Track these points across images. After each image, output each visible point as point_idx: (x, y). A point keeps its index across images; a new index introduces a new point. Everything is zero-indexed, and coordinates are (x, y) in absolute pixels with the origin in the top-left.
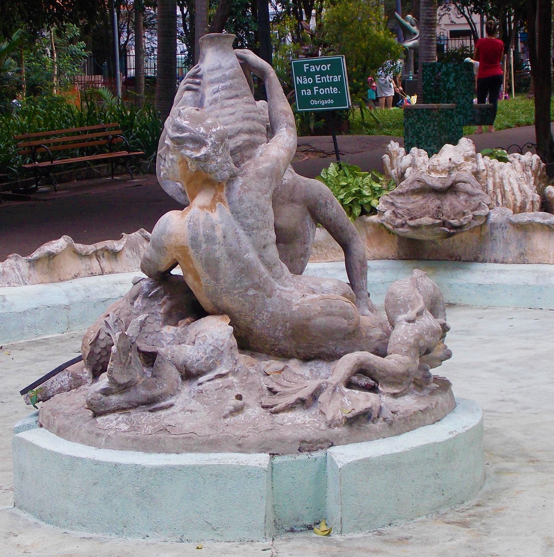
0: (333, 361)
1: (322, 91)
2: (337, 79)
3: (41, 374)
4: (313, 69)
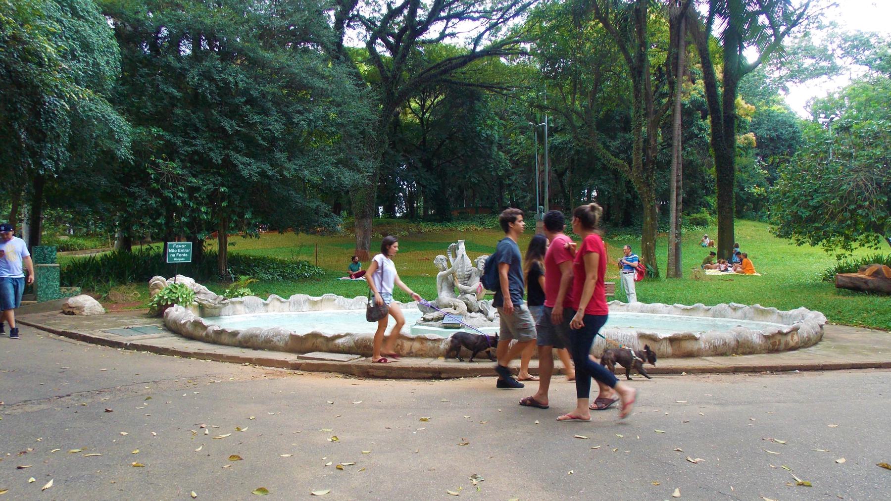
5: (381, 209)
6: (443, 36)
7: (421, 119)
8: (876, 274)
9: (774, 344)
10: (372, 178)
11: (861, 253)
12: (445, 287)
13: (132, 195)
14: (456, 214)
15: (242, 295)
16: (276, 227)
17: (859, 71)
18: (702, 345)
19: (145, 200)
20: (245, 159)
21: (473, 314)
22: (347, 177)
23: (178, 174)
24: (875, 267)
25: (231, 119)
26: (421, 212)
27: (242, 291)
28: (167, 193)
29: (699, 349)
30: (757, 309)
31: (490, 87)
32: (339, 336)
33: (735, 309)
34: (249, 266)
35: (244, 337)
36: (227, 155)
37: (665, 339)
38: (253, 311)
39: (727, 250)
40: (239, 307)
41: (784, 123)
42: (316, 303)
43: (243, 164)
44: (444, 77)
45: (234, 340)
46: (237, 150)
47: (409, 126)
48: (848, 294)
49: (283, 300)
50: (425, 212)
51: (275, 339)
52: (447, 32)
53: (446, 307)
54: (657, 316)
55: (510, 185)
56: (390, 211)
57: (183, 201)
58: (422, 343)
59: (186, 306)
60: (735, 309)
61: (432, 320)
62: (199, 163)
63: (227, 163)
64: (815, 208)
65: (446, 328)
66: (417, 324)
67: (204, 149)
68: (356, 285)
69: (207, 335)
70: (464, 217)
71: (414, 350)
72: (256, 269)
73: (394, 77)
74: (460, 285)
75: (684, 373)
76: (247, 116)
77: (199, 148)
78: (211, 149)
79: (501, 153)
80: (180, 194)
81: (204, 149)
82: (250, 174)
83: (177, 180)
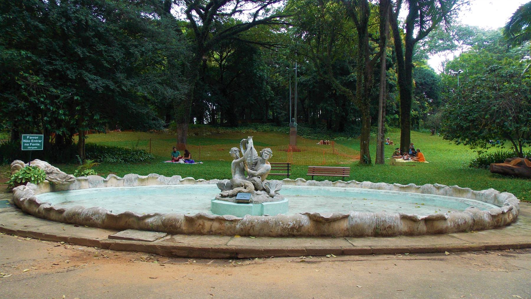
0: (413, 217)
1: (33, 145)
2: (40, 141)
3: (388, 240)
4: (31, 138)
5: (195, 119)
6: (234, 12)
7: (220, 64)
8: (520, 164)
9: (498, 222)
10: (188, 95)
11: (492, 150)
12: (237, 172)
13: (7, 100)
14: (240, 122)
15: (87, 175)
16: (126, 128)
17: (467, 48)
18: (449, 224)
19: (16, 104)
20: (93, 77)
21: (259, 192)
22: (169, 92)
23: (40, 85)
24: (519, 160)
25: (83, 47)
26: (219, 121)
27: (87, 171)
28: (32, 99)
29: (447, 227)
30: (455, 189)
31: (263, 45)
32: (149, 216)
33: (438, 188)
34: (102, 153)
35: (68, 215)
36: (80, 74)
37: (422, 219)
38: (96, 186)
39: (406, 148)
40: (84, 184)
41: (429, 75)
42: (143, 180)
43: (92, 80)
44: (235, 36)
45: (60, 217)
46: (87, 70)
47: (213, 69)
48: (500, 177)
49: (119, 178)
50: (222, 121)
51: (94, 218)
52: (237, 10)
53: (238, 186)
54: (382, 192)
55: (272, 106)
56: (200, 120)
57: (46, 106)
58: (221, 223)
59: (38, 184)
60: (438, 188)
61: (228, 196)
62: (59, 78)
63: (82, 81)
64: (472, 121)
65: (238, 203)
66: (216, 199)
67: (62, 68)
68: (175, 166)
69: (39, 212)
70: (245, 124)
71: (213, 229)
72: (106, 155)
73: (203, 34)
74: (249, 170)
75: (447, 253)
76: (95, 46)
77: (59, 67)
78: (68, 69)
79: (268, 86)
80: (42, 99)
81: (62, 68)
82: (97, 87)
83: (40, 90)
